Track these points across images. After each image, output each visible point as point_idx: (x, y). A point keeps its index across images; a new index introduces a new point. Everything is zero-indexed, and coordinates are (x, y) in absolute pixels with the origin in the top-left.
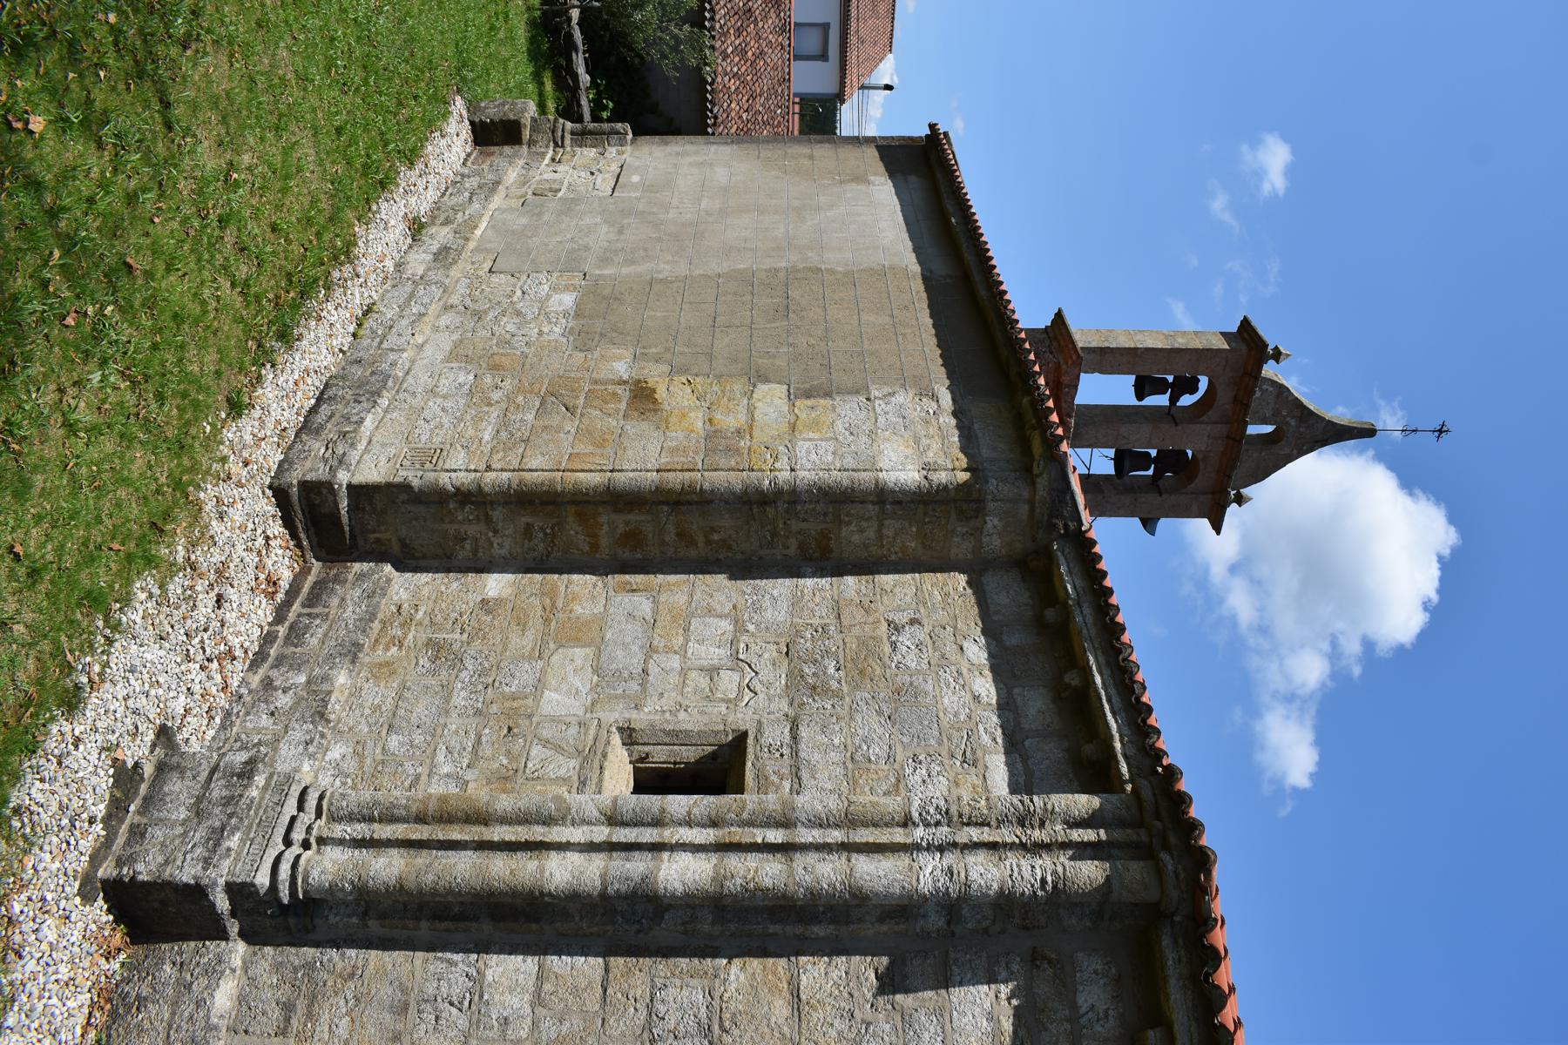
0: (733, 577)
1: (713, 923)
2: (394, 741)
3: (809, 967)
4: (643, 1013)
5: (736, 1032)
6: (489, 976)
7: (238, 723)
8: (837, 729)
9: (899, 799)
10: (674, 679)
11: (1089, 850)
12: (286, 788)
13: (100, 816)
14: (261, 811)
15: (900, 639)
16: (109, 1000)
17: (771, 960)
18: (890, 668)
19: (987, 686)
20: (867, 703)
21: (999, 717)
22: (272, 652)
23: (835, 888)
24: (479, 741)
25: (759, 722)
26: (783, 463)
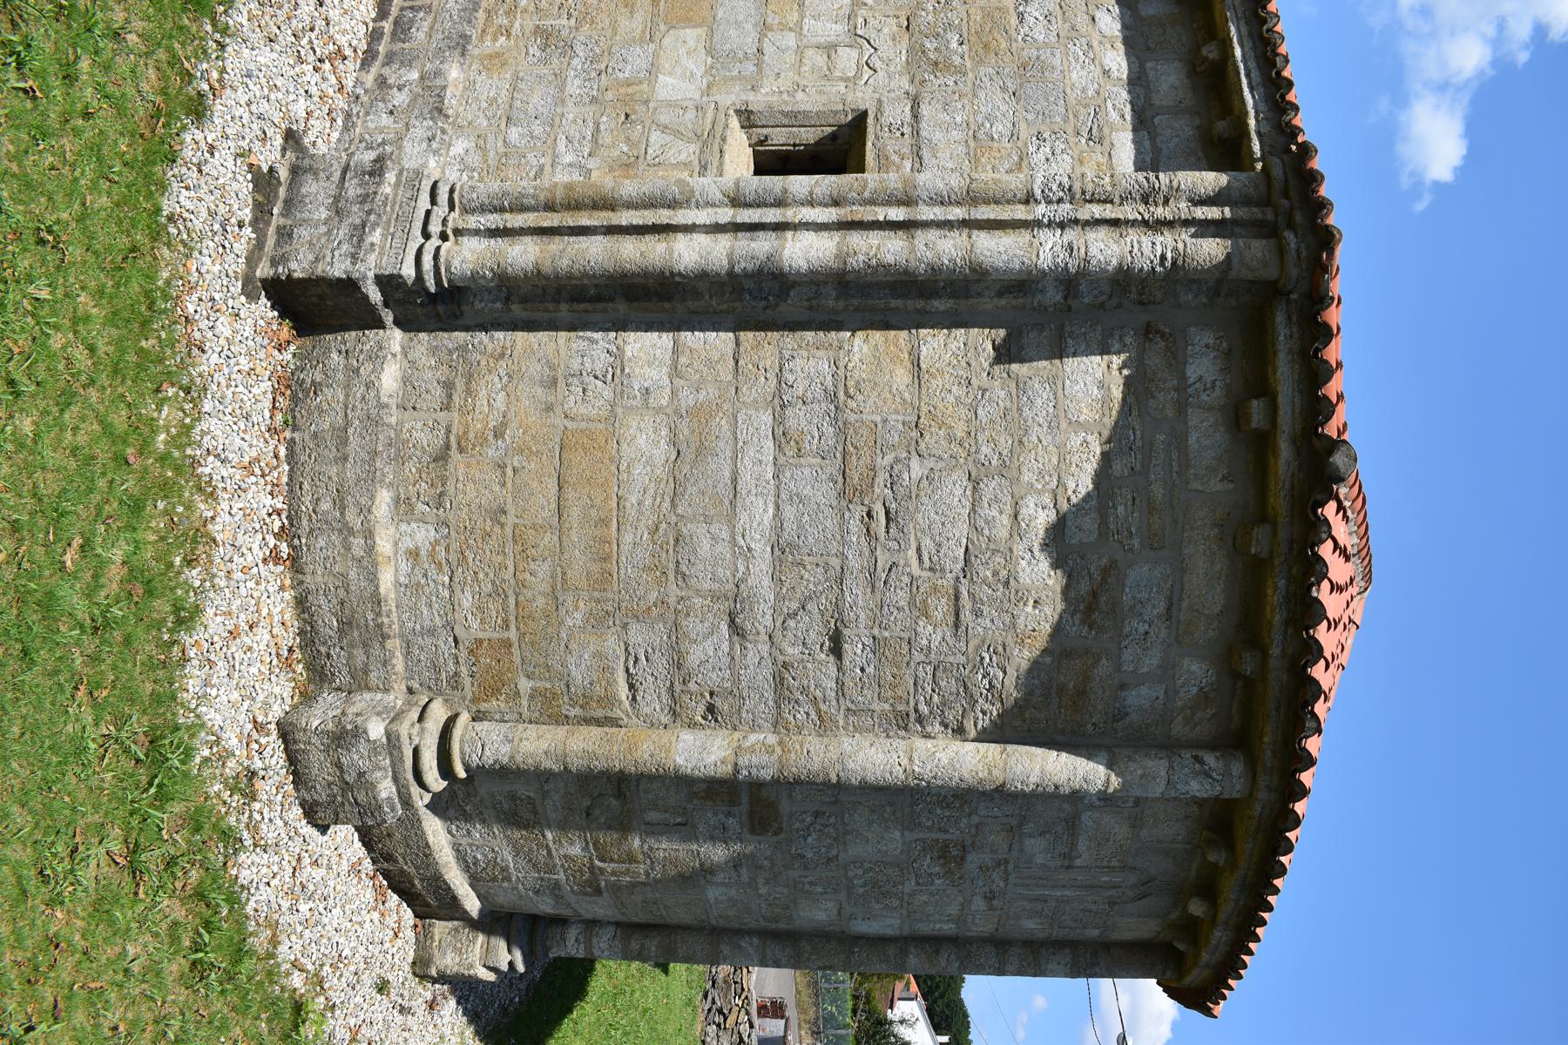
1: (837, 299)
2: (514, 134)
3: (929, 339)
4: (773, 382)
5: (860, 398)
7: (359, 123)
9: (1021, 176)
10: (790, 58)
11: (1212, 229)
13: (247, 221)
14: (397, 207)
15: (1028, 10)
16: (288, 387)
17: (893, 333)
18: (1016, 41)
20: (991, 79)
21: (1129, 92)
22: (381, 49)
23: (955, 264)
24: (597, 129)
25: (879, 101)
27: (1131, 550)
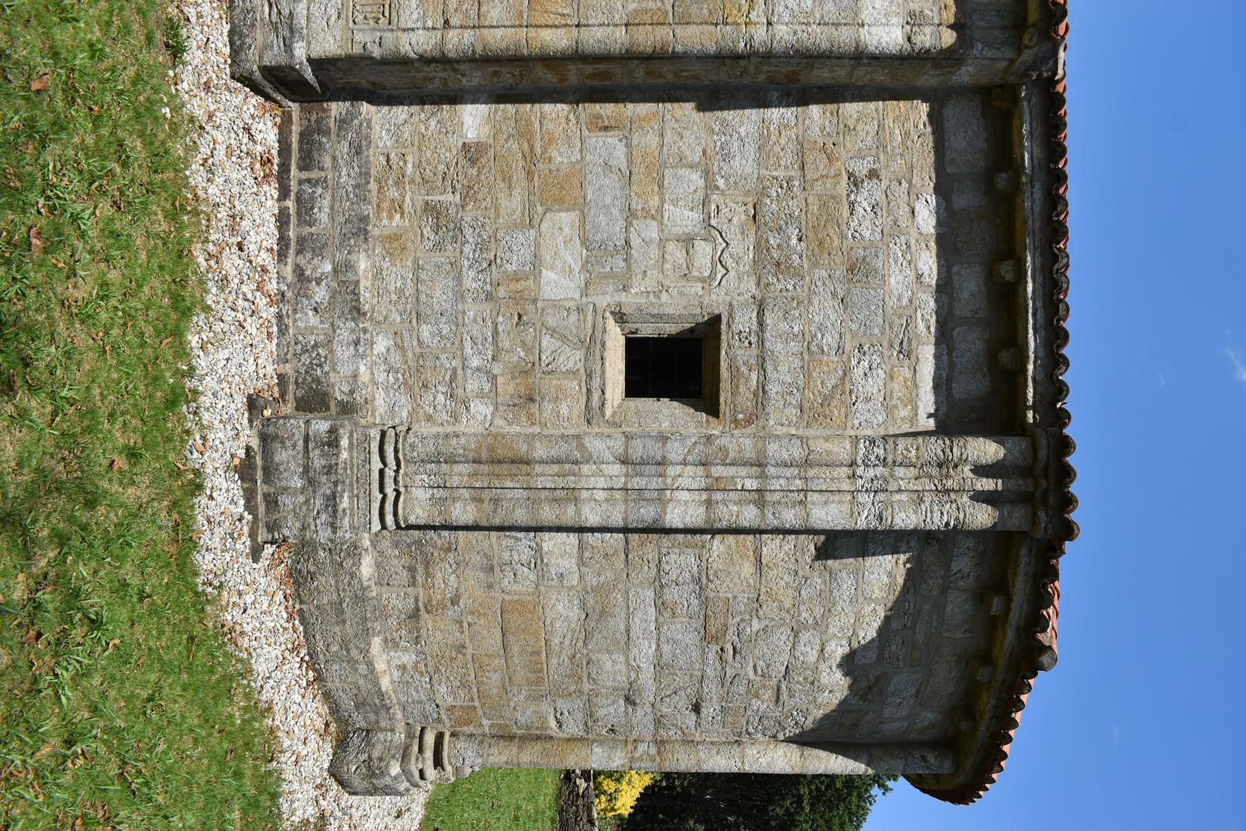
0: (701, 108)
2: (426, 331)
3: (769, 542)
5: (718, 582)
6: (545, 547)
8: (797, 315)
10: (654, 253)
12: (367, 446)
14: (355, 469)
19: (931, 262)
21: (936, 301)
24: (496, 332)
26: (758, 15)
27: (897, 667)
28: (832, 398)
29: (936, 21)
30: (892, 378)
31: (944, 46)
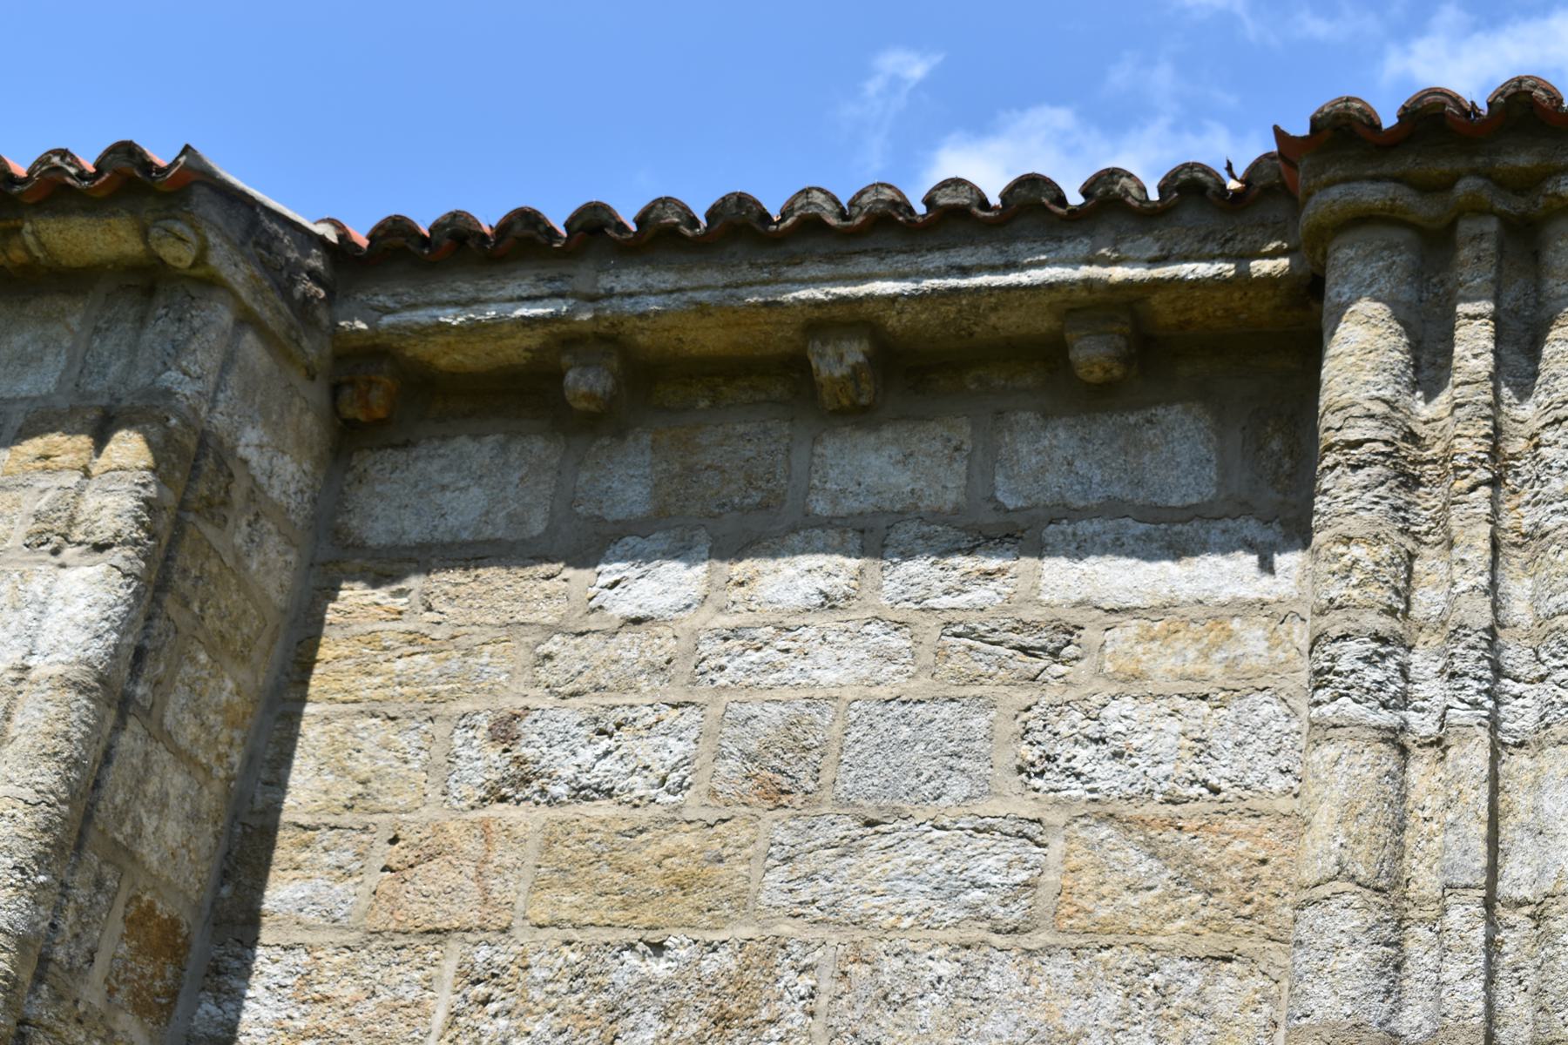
8: (898, 963)
18: (678, 808)
20: (809, 878)
21: (907, 555)
28: (1188, 857)
29: (73, 479)
30: (1136, 677)
31: (146, 459)
